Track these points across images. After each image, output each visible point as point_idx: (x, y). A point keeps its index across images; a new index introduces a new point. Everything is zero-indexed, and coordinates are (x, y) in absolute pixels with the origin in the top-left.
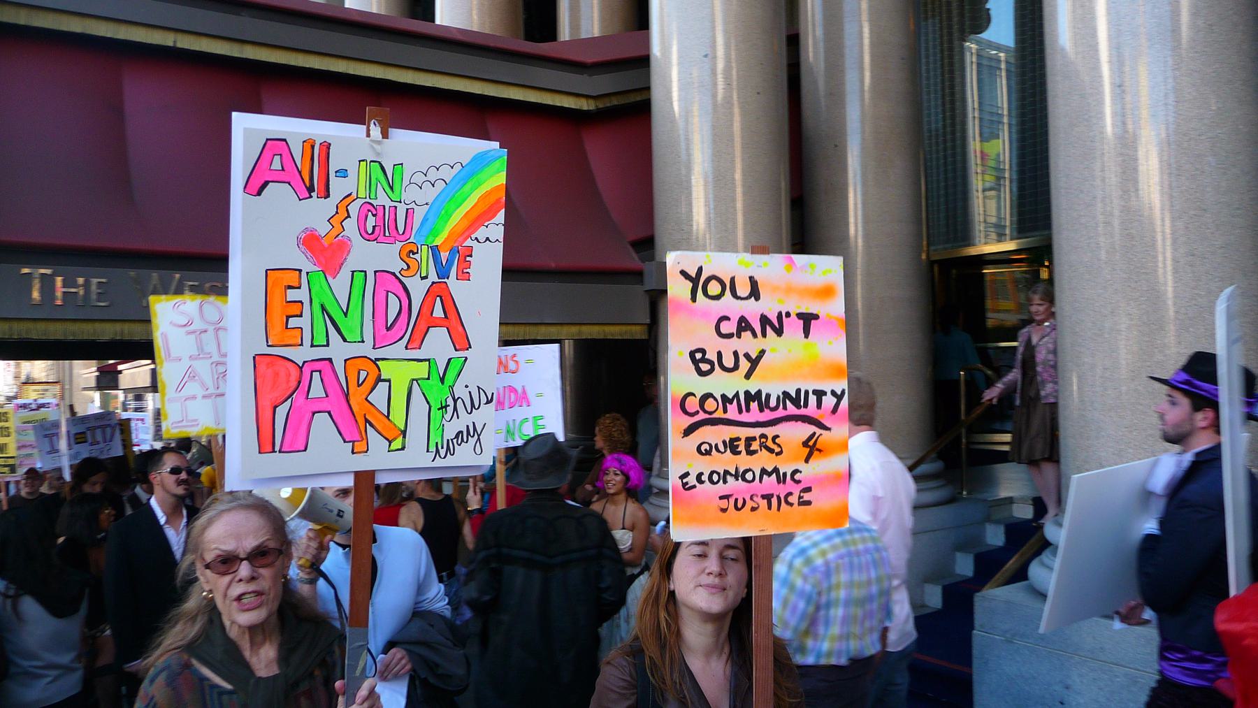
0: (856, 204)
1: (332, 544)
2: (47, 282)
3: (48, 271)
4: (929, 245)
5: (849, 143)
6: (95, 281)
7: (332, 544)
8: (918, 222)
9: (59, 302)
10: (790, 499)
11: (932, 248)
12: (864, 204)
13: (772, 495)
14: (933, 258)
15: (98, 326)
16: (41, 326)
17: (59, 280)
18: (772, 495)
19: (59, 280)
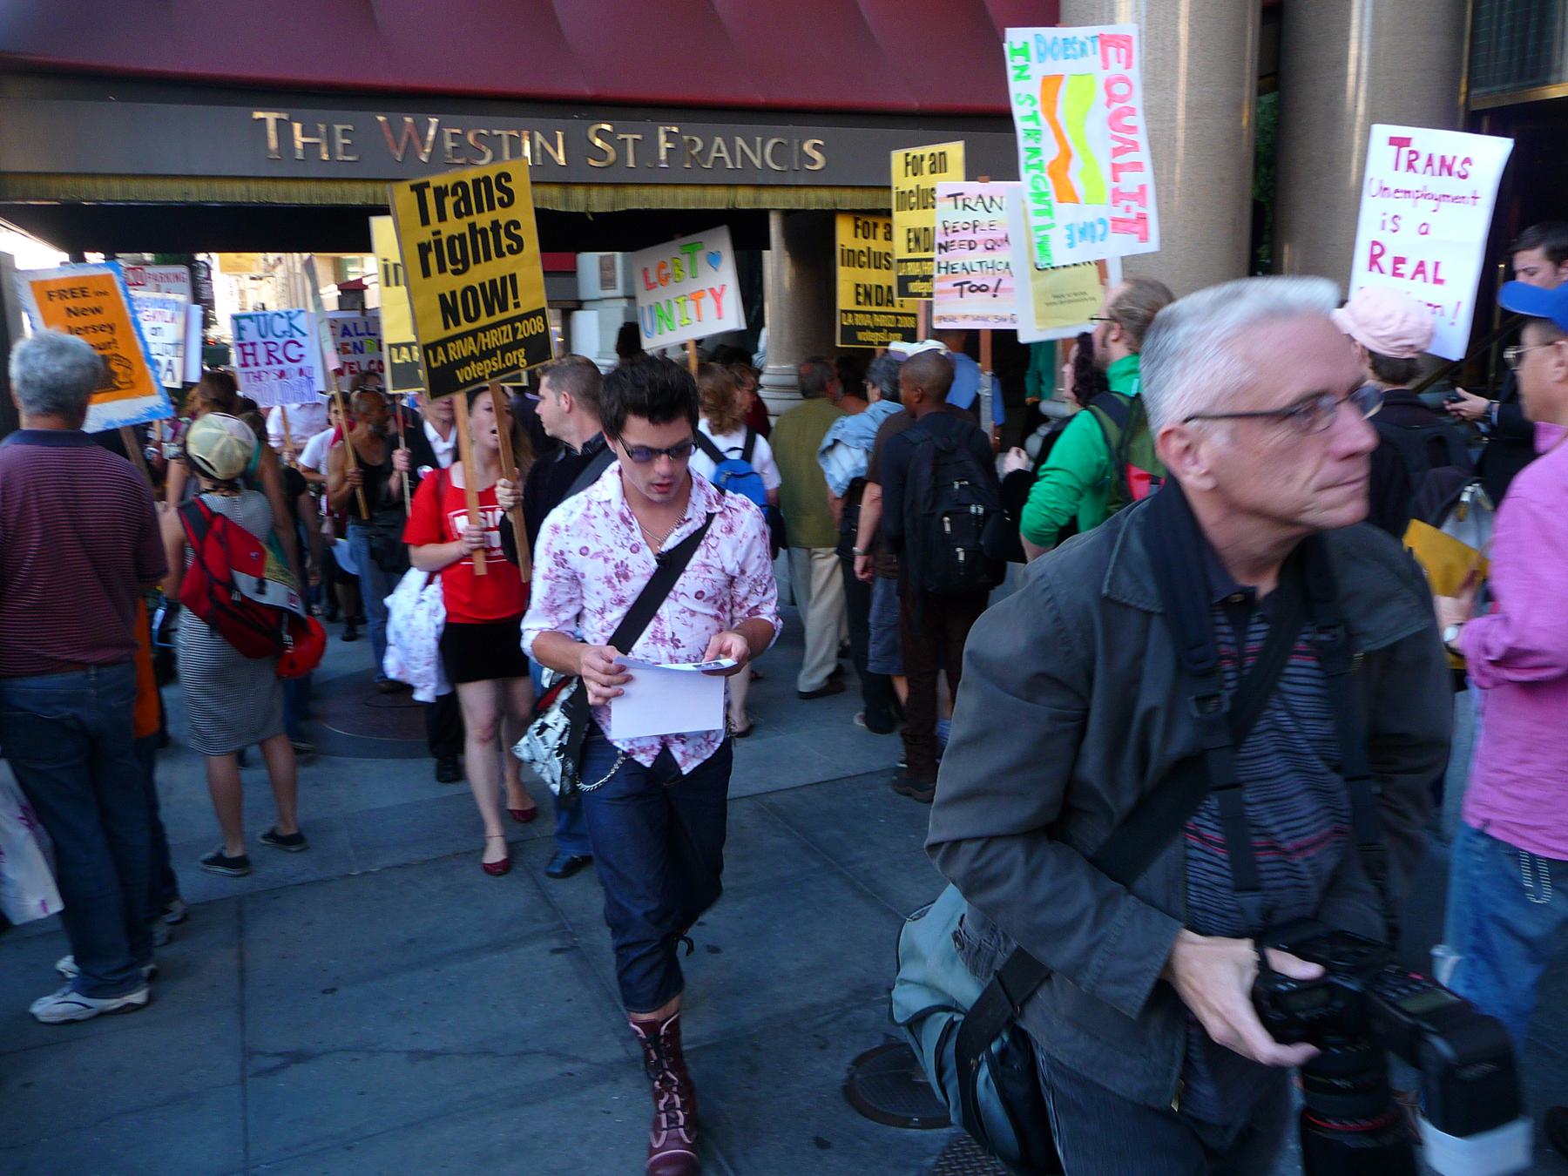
0: (1358, 74)
1: (204, 497)
2: (284, 128)
3: (284, 116)
4: (1469, 88)
5: (1196, 1011)
6: (338, 128)
7: (204, 497)
8: (1459, 36)
9: (300, 156)
10: (1403, 268)
11: (1474, 92)
12: (1374, 57)
13: (1114, 165)
14: (1475, 108)
15: (346, 186)
16: (282, 187)
17: (297, 127)
18: (1114, 165)
19: (297, 127)
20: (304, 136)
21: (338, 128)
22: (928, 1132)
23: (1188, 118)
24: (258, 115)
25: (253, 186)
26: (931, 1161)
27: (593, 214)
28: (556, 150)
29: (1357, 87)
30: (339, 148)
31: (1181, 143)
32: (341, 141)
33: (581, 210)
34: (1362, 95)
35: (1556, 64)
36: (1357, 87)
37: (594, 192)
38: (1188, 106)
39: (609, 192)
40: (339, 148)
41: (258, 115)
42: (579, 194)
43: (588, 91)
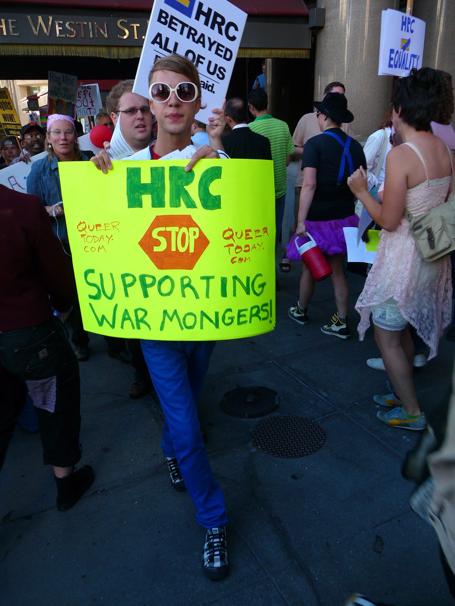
20: (59, 26)
21: (10, 21)
22: (251, 419)
23: (370, 17)
24: (133, 25)
25: (29, 48)
26: (251, 430)
27: (120, 60)
28: (105, 33)
29: (441, 12)
30: (11, 30)
31: (366, 28)
32: (11, 27)
33: (116, 58)
34: (443, 15)
35: (262, 112)
36: (441, 12)
37: (121, 50)
38: (370, 12)
39: (127, 50)
40: (11, 30)
41: (133, 25)
42: (114, 51)
43: (116, 4)
